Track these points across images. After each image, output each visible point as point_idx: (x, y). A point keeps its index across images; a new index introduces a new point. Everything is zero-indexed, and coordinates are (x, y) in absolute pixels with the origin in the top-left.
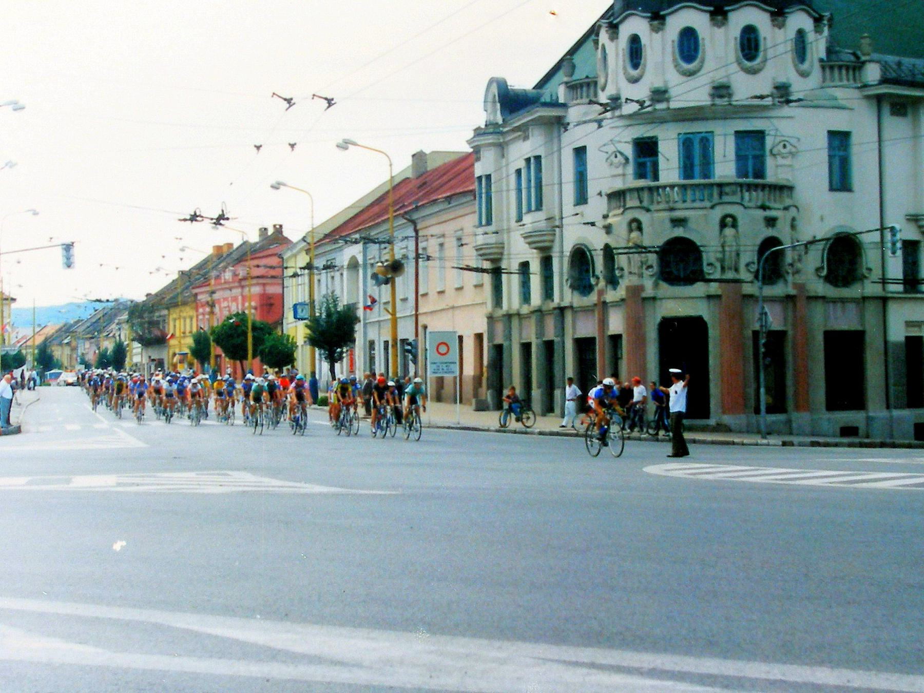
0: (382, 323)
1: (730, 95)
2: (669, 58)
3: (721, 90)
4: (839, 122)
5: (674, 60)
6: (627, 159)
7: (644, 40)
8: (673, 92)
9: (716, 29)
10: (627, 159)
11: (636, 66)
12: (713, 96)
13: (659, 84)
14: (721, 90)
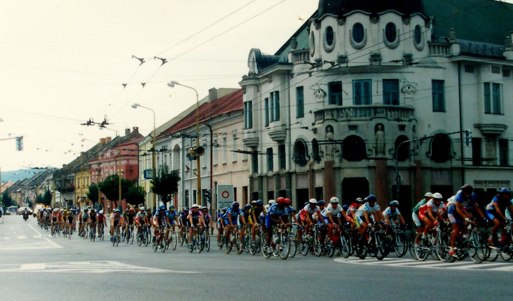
0: (192, 180)
1: (380, 60)
2: (348, 40)
3: (376, 57)
4: (438, 75)
5: (351, 41)
6: (325, 93)
7: (335, 30)
8: (350, 58)
9: (373, 24)
10: (325, 93)
11: (330, 43)
12: (371, 60)
13: (342, 53)
14: (376, 57)
